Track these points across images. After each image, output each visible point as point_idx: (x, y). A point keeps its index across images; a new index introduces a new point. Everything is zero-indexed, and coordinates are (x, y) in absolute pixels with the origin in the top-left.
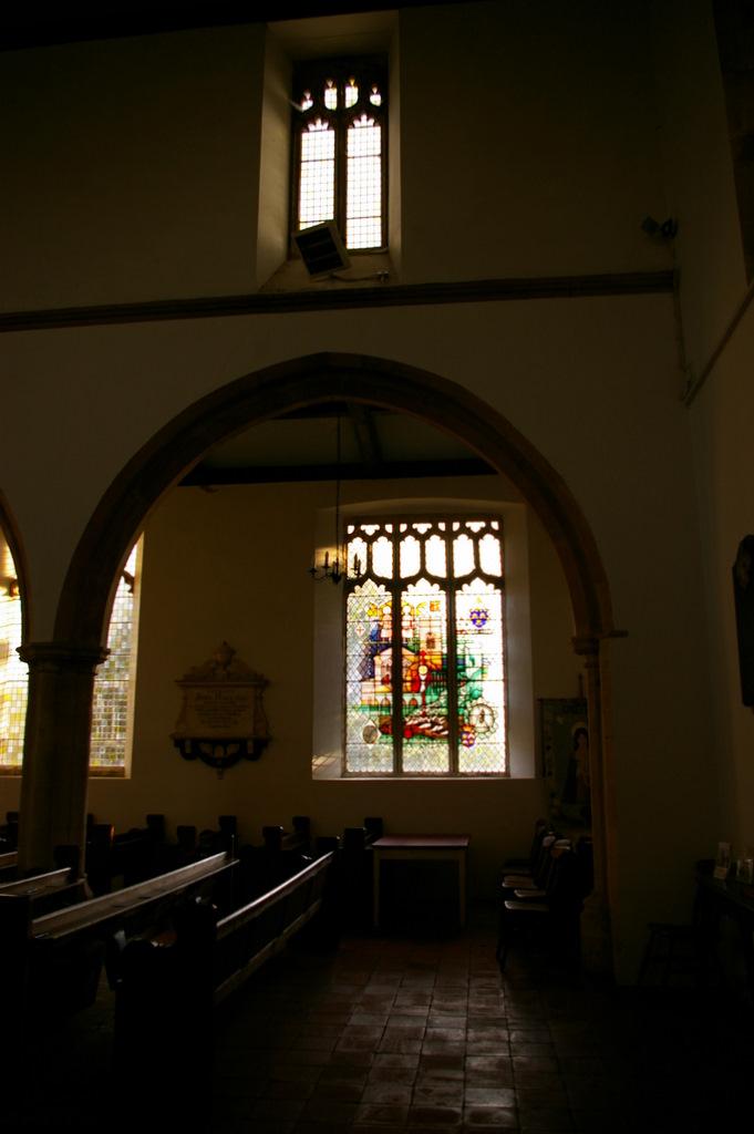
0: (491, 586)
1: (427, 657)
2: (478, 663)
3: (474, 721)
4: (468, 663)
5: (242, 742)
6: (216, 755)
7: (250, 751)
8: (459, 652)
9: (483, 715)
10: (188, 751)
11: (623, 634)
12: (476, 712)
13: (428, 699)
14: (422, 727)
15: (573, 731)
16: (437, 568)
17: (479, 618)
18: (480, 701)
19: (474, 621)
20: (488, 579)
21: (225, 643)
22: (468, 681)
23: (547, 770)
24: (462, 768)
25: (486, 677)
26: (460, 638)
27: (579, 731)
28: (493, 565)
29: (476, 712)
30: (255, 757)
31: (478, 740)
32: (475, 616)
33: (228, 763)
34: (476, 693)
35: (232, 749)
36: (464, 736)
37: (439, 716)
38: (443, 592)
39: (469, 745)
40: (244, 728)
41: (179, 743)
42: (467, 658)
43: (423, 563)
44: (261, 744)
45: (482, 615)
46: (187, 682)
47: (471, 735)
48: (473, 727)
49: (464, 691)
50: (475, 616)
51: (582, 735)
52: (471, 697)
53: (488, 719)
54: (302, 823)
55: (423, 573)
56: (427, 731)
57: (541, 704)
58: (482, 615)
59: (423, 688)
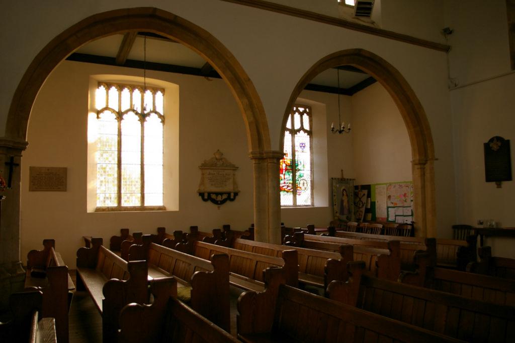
0: (306, 134)
1: (285, 160)
2: (302, 164)
3: (301, 185)
4: (299, 163)
5: (229, 194)
6: (218, 199)
7: (232, 197)
8: (296, 159)
9: (304, 184)
10: (206, 197)
11: (437, 159)
12: (302, 182)
13: (286, 177)
14: (284, 188)
15: (342, 190)
16: (114, 105)
17: (303, 146)
18: (303, 178)
19: (301, 147)
20: (305, 131)
21: (218, 150)
22: (299, 170)
23: (334, 203)
24: (298, 204)
25: (305, 169)
26: (296, 153)
27: (344, 190)
28: (307, 126)
29: (302, 182)
30: (232, 200)
31: (302, 193)
32: (301, 145)
33: (223, 202)
34: (302, 175)
35: (225, 197)
36: (298, 191)
37: (290, 183)
38: (309, 136)
39: (299, 195)
40: (229, 188)
41: (201, 194)
42: (299, 161)
43: (107, 102)
44: (236, 194)
45: (304, 145)
46: (204, 166)
47: (300, 191)
48: (301, 188)
49: (298, 174)
50: (301, 145)
51: (344, 191)
52: (300, 176)
53: (305, 185)
54: (194, 229)
55: (302, 128)
56: (286, 190)
57: (332, 180)
58: (304, 145)
59: (284, 172)
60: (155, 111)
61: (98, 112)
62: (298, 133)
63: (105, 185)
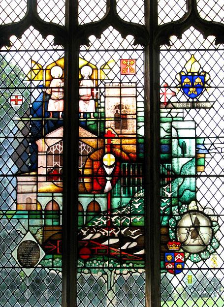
4: (176, 150)
12: (187, 222)
18: (192, 206)
22: (177, 176)
47: (179, 257)
48: (182, 244)
52: (180, 199)
53: (204, 233)
60: (112, 19)
61: (32, 19)
62: (173, 38)
63: (135, 50)
